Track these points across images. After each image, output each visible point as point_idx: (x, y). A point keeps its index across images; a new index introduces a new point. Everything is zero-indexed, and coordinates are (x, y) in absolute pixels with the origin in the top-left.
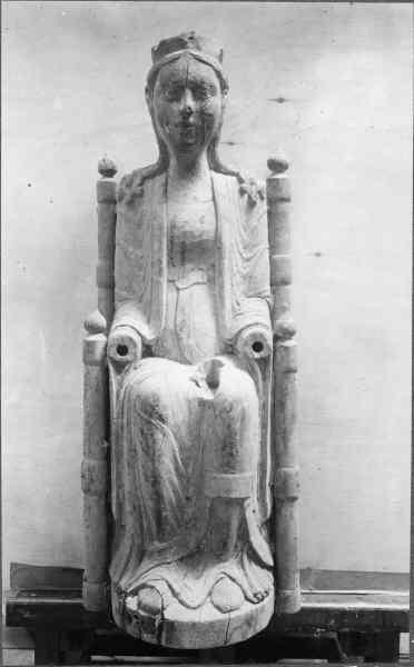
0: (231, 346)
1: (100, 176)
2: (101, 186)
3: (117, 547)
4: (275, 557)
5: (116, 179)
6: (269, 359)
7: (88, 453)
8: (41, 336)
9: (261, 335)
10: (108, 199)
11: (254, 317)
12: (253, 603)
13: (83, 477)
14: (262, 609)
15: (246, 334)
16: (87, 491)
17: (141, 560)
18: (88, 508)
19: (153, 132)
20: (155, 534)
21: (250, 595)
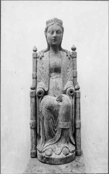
0: (65, 92)
1: (33, 52)
2: (33, 54)
3: (34, 134)
4: (75, 142)
5: (37, 52)
6: (74, 94)
7: (32, 119)
8: (34, 139)
9: (72, 89)
10: (36, 58)
11: (69, 85)
12: (72, 153)
13: (30, 124)
14: (73, 154)
15: (68, 90)
16: (31, 128)
17: (45, 143)
18: (33, 82)
19: (46, 40)
20: (38, 136)
21: (71, 151)
